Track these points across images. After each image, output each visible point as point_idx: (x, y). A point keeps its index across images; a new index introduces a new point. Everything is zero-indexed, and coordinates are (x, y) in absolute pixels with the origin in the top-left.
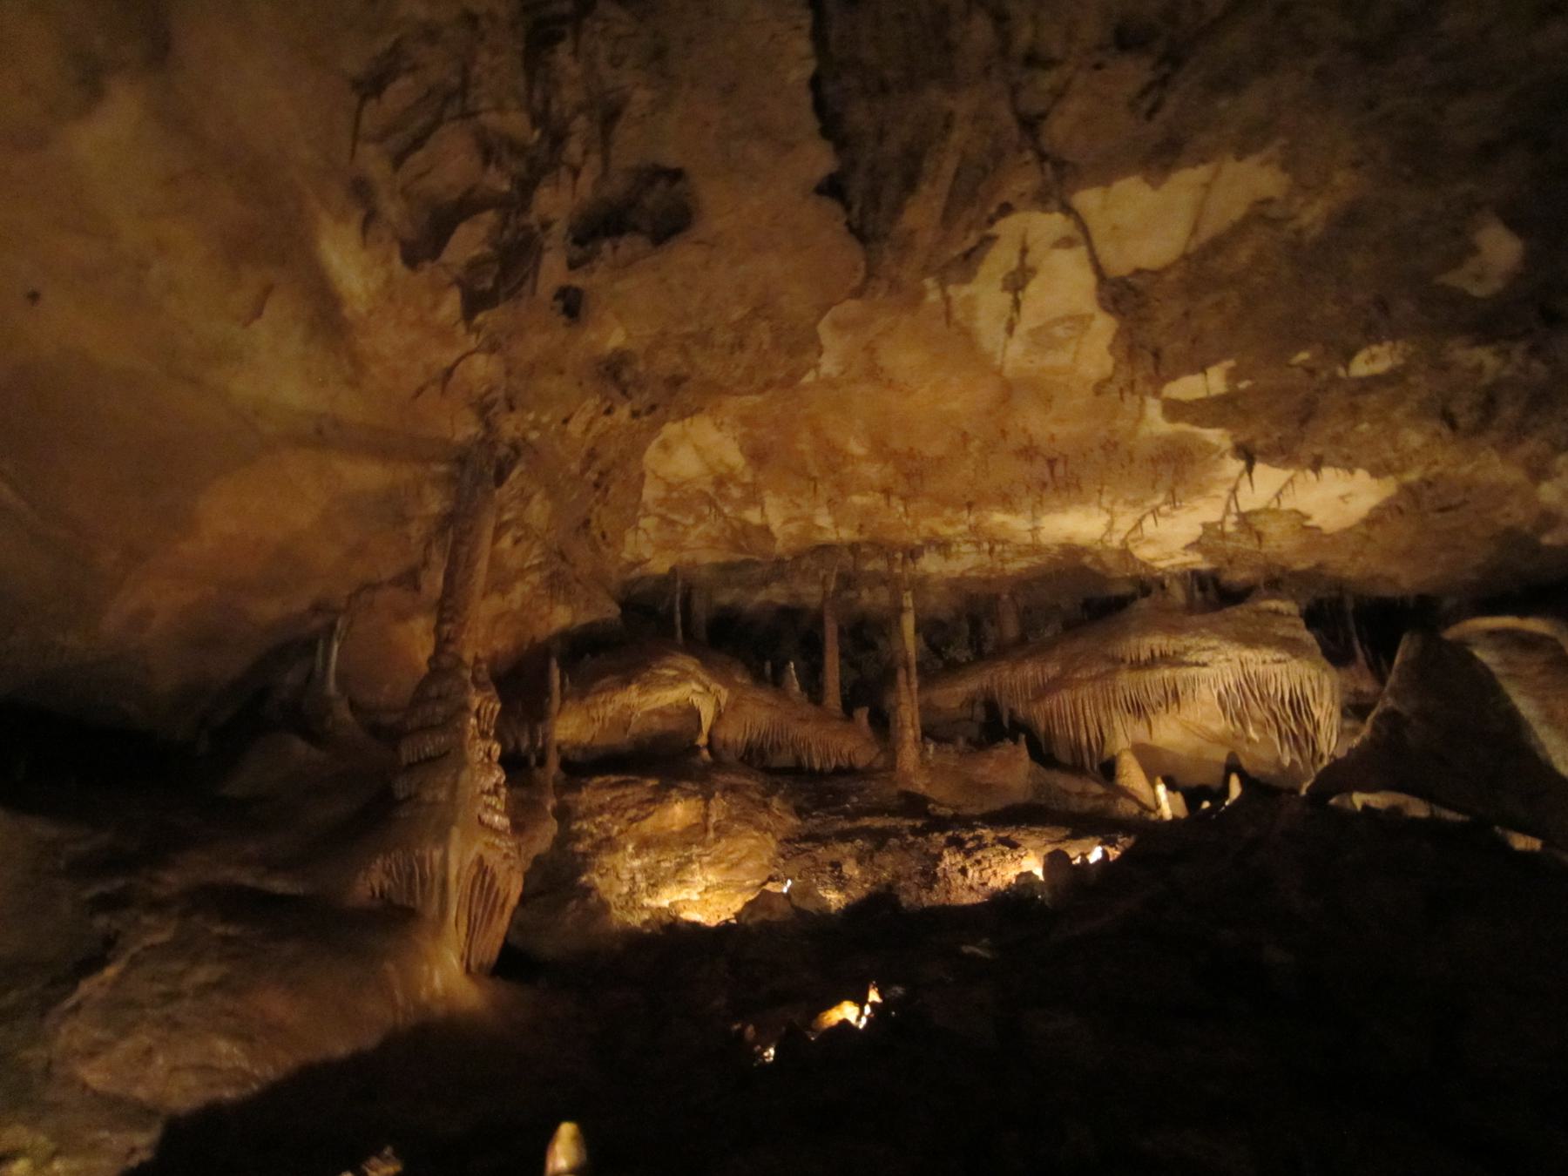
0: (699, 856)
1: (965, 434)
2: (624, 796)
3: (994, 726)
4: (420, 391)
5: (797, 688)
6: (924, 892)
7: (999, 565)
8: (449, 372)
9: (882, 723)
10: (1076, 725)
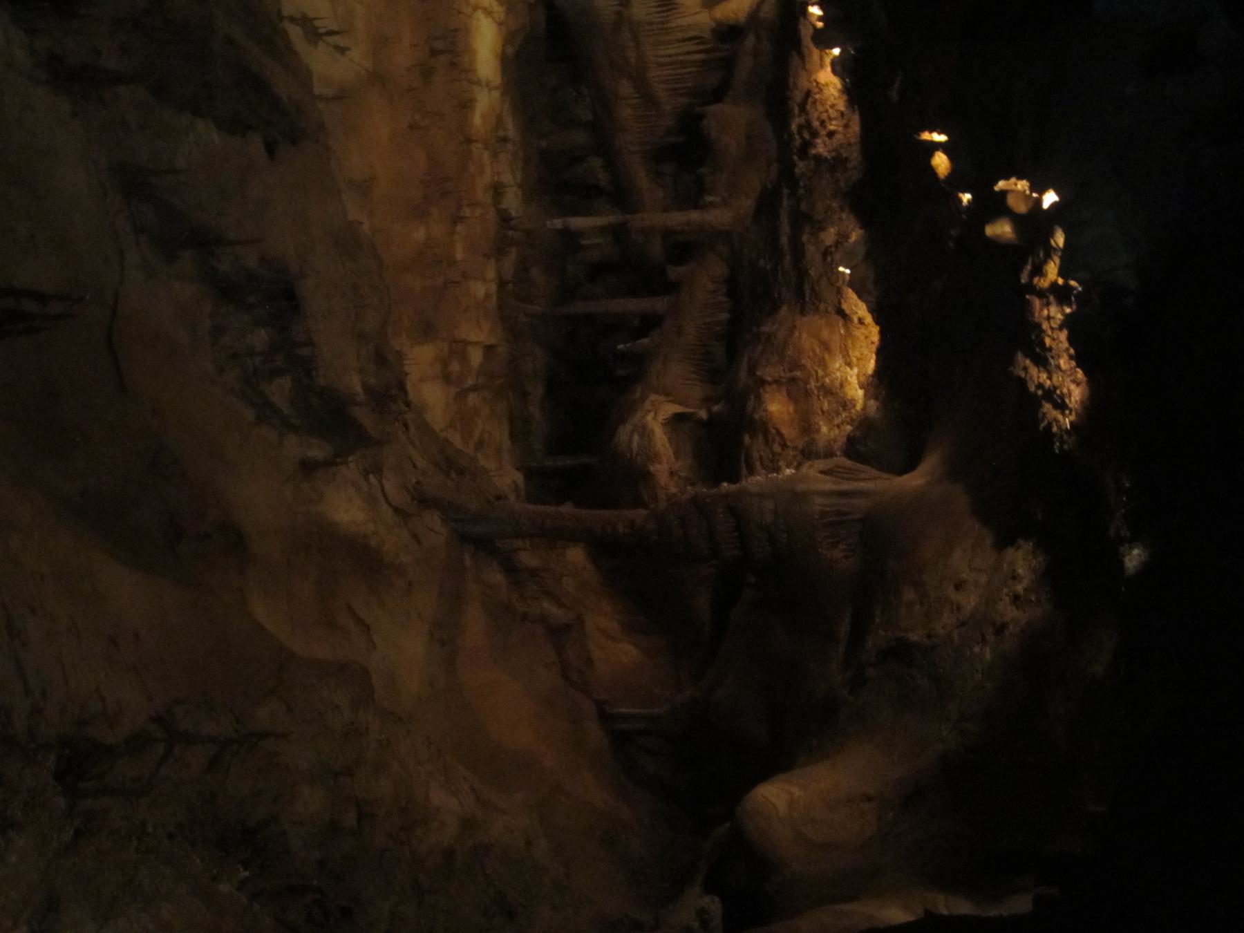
0: (817, 380)
1: (411, 127)
2: (761, 458)
3: (687, 153)
4: (415, 536)
5: (646, 341)
6: (850, 165)
7: (510, 146)
8: (397, 510)
9: (683, 248)
10: (683, 64)
